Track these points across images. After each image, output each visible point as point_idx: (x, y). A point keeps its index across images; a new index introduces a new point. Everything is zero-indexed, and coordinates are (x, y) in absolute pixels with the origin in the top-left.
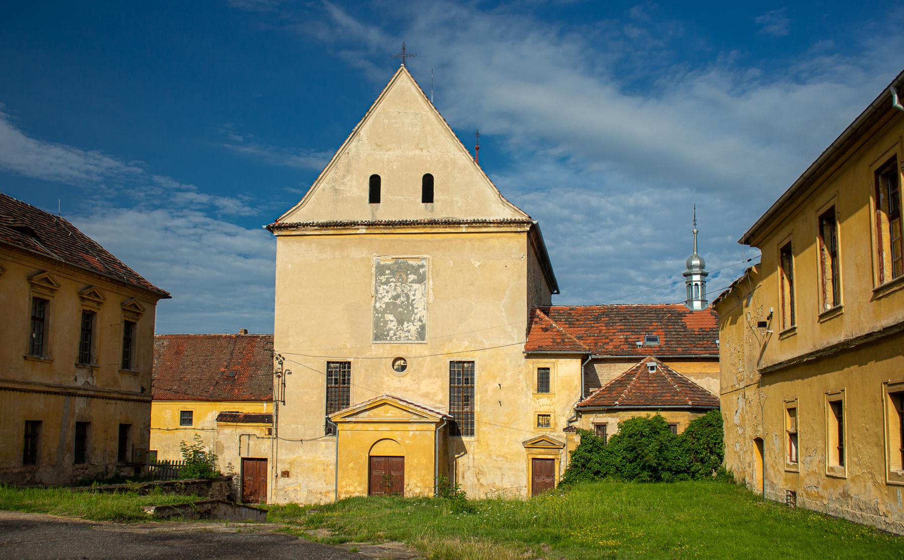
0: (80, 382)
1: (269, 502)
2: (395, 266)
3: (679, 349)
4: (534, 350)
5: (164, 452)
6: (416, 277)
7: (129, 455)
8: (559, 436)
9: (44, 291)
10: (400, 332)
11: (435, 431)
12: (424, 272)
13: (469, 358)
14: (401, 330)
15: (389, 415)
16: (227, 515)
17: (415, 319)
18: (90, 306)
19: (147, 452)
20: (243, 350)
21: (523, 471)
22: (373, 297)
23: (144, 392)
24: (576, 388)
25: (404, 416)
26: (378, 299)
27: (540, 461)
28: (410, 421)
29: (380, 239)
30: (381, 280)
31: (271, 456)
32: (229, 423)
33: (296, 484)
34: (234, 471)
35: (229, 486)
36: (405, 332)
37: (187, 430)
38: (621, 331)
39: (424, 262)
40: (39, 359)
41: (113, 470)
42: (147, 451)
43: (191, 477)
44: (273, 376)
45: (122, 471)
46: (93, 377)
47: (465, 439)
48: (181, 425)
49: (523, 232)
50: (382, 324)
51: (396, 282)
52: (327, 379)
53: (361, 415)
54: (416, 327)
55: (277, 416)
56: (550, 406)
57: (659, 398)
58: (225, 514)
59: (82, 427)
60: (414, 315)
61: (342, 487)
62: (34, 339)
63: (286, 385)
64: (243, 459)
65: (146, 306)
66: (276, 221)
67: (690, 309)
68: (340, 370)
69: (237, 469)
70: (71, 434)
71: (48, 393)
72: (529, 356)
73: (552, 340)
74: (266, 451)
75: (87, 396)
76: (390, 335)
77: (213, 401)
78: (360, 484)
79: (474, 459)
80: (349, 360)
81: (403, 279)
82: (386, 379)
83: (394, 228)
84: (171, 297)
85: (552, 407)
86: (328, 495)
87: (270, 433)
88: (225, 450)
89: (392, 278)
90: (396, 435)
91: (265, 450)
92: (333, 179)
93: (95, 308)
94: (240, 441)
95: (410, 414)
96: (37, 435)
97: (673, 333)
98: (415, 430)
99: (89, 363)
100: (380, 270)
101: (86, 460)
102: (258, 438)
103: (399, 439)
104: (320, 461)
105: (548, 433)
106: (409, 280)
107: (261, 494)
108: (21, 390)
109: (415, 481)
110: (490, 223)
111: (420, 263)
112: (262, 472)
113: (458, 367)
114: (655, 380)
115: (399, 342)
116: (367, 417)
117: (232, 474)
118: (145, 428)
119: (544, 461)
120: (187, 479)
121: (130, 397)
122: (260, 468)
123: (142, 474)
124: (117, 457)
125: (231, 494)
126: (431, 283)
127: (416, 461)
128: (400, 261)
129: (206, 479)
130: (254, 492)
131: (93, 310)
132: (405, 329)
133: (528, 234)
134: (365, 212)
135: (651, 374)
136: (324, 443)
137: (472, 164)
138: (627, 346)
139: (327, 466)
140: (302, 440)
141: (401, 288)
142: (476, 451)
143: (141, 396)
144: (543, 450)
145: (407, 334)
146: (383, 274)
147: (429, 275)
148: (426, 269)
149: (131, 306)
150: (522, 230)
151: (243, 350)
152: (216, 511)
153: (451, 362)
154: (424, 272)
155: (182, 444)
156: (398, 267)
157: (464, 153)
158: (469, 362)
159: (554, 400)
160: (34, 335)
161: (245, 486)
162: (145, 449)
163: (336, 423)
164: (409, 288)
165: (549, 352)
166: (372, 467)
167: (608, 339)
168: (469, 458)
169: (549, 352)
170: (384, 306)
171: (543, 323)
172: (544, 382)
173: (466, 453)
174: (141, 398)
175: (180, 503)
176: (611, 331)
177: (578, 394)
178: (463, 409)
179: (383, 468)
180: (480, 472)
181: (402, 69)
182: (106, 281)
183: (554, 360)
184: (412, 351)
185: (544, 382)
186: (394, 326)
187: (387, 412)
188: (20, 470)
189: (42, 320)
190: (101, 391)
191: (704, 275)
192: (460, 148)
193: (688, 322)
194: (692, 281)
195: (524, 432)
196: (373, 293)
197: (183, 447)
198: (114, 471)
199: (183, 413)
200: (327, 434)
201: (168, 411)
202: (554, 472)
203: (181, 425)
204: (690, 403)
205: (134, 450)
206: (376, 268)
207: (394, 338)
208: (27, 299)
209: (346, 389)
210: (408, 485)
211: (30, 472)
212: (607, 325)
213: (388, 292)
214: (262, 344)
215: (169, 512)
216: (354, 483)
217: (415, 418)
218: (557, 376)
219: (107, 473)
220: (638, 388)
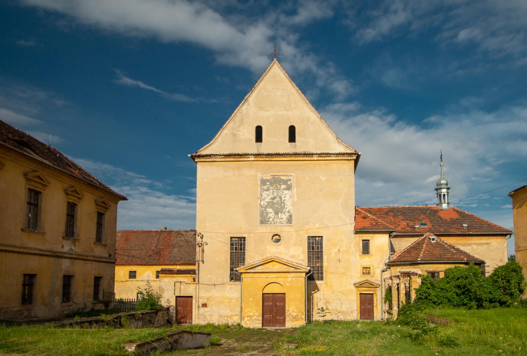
0: (66, 249)
1: (194, 322)
2: (273, 180)
3: (442, 230)
4: (360, 229)
5: (119, 294)
6: (285, 186)
7: (101, 296)
8: (376, 280)
9: (37, 185)
10: (276, 219)
11: (305, 278)
12: (291, 184)
13: (319, 234)
14: (277, 218)
15: (275, 268)
16: (188, 341)
17: (285, 211)
18: (72, 199)
19: (112, 294)
20: (165, 238)
21: (354, 301)
22: (259, 198)
23: (111, 257)
24: (386, 251)
25: (285, 268)
26: (262, 200)
27: (364, 295)
28: (290, 271)
29: (263, 164)
30: (264, 188)
31: (195, 295)
32: (167, 275)
33: (211, 311)
34: (171, 304)
35: (168, 314)
36: (280, 219)
37: (133, 282)
38: (403, 220)
39: (291, 178)
40: (34, 231)
41: (90, 306)
42: (113, 293)
43: (145, 309)
44: (196, 246)
45: (96, 307)
46: (75, 246)
47: (318, 282)
48: (129, 278)
49: (352, 160)
50: (265, 214)
51: (273, 189)
52: (231, 248)
53: (257, 268)
54: (286, 216)
55: (199, 270)
56: (370, 262)
57: (444, 256)
58: (187, 341)
59: (68, 279)
60: (285, 209)
61: (245, 313)
62: (30, 217)
63: (204, 251)
64: (177, 297)
65: (112, 204)
66: (196, 153)
67: (441, 208)
68: (238, 242)
69: (173, 303)
70: (59, 284)
71: (41, 255)
72: (357, 232)
73: (370, 224)
74: (192, 291)
75: (72, 258)
76: (270, 221)
77: (149, 265)
78: (257, 311)
79: (323, 294)
80: (244, 236)
81: (278, 188)
82: (268, 247)
83: (272, 157)
84: (127, 200)
85: (372, 263)
86: (232, 317)
87: (194, 281)
88: (165, 291)
89: (270, 187)
90: (280, 280)
91: (191, 291)
92: (232, 127)
93: (76, 201)
94: (175, 286)
95: (289, 267)
96: (33, 284)
97: (435, 221)
98: (292, 277)
99: (73, 236)
100: (263, 182)
101: (71, 300)
102: (186, 284)
103: (282, 283)
104: (227, 297)
105: (369, 278)
106: (282, 188)
107: (188, 317)
108: (19, 253)
109: (293, 308)
110: (332, 154)
111: (288, 178)
112: (189, 304)
113: (313, 240)
114: (437, 246)
115: (276, 225)
116: (261, 269)
117: (170, 306)
118: (111, 279)
119: (366, 295)
120: (142, 311)
121: (101, 260)
122: (187, 302)
123: (110, 308)
124: (93, 298)
125: (169, 318)
126: (295, 190)
127: (293, 296)
128: (276, 177)
129: (155, 310)
130: (183, 316)
131: (75, 202)
132: (280, 217)
133: (355, 161)
134: (253, 148)
135: (433, 243)
136: (229, 286)
137: (320, 120)
138: (409, 228)
139: (231, 300)
140: (215, 285)
141: (277, 193)
142: (325, 289)
143: (108, 259)
144: (366, 289)
145: (281, 220)
146: (265, 184)
147: (294, 185)
148: (292, 182)
149: (101, 202)
150: (351, 158)
151: (165, 238)
152: (181, 339)
153: (308, 237)
154: (291, 184)
155: (138, 288)
156: (274, 181)
157: (314, 113)
158: (319, 237)
159: (373, 258)
160: (30, 215)
161: (178, 313)
162: (111, 292)
163: (241, 273)
164: (281, 193)
165: (370, 230)
166: (264, 300)
167: (396, 224)
168: (320, 293)
169: (370, 230)
170: (266, 204)
171: (362, 214)
172: (366, 248)
173: (319, 290)
174: (109, 261)
175: (156, 337)
176: (397, 220)
177: (387, 255)
178: (316, 264)
179: (271, 301)
180: (327, 302)
181: (275, 62)
182: (84, 184)
183: (372, 235)
184: (285, 230)
185: (366, 248)
186: (273, 215)
187: (274, 266)
188: (18, 309)
189: (36, 206)
190: (81, 255)
191: (448, 189)
192: (312, 110)
193: (441, 214)
194: (441, 192)
195: (355, 278)
196: (259, 196)
197: (139, 290)
198: (90, 306)
199: (130, 272)
200: (231, 280)
201: (121, 271)
202: (373, 301)
203: (129, 278)
204: (465, 259)
205: (104, 293)
206: (261, 181)
207: (273, 223)
208: (24, 189)
209: (242, 253)
210: (288, 311)
211: (27, 310)
212: (394, 217)
213: (268, 195)
214: (176, 235)
215: (148, 346)
216: (253, 310)
217: (292, 269)
218: (374, 245)
219: (86, 308)
220: (429, 251)
